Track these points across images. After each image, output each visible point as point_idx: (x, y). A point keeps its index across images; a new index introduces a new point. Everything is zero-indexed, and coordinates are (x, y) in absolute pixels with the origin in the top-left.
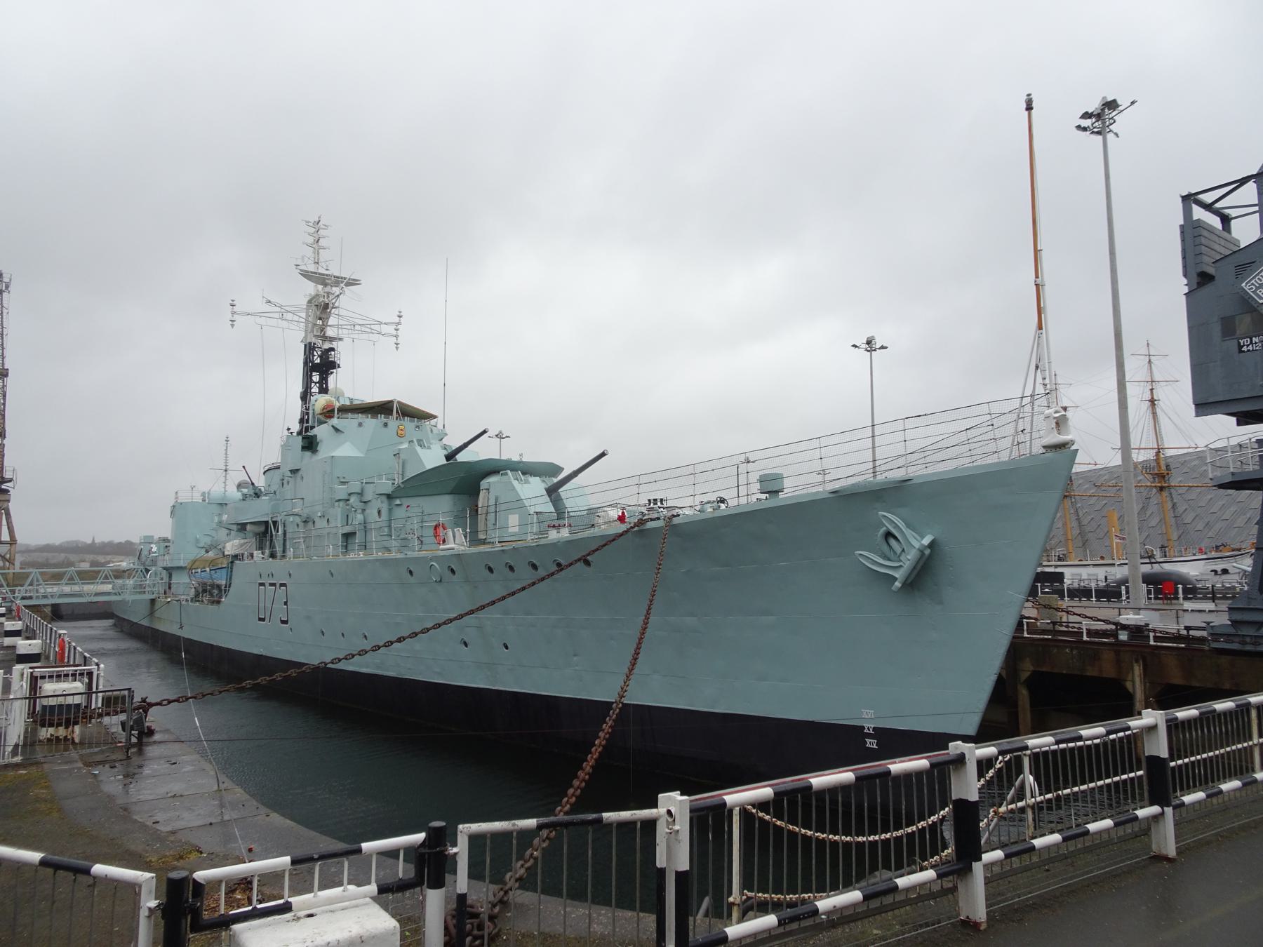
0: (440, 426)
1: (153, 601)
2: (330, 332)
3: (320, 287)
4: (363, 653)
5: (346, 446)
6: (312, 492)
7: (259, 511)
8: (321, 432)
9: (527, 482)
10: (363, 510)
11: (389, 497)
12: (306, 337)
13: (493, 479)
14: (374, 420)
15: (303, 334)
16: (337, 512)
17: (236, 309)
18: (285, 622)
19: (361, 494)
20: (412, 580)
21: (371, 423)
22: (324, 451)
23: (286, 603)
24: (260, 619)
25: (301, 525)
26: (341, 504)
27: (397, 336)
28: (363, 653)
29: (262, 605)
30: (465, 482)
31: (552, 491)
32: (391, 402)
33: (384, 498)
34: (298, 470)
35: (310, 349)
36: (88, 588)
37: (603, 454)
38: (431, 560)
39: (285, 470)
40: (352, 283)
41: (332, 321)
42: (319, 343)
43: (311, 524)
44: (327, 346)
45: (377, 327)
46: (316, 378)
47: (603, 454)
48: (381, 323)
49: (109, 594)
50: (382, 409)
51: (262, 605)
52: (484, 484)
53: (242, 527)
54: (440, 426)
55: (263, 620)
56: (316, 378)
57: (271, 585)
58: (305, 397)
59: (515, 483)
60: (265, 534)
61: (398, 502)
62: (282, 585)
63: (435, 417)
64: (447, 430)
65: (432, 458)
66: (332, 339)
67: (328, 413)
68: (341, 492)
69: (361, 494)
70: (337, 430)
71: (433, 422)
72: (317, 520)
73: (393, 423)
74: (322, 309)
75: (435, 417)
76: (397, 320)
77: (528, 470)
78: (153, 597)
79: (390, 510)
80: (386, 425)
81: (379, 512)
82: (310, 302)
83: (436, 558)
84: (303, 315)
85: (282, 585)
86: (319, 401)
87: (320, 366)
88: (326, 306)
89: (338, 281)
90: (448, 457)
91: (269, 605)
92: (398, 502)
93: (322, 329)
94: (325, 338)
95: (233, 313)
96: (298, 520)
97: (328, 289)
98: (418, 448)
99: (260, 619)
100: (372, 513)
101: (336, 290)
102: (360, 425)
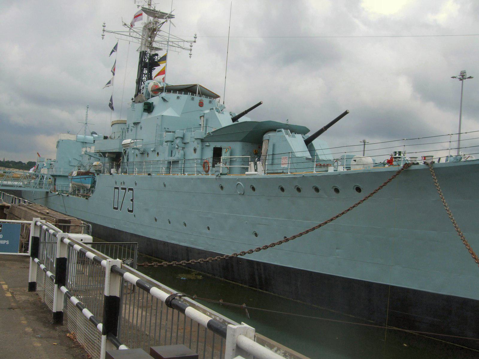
0: (221, 103)
1: (47, 193)
2: (155, 45)
3: (151, 19)
4: (251, 252)
5: (170, 109)
6: (147, 134)
7: (113, 146)
8: (155, 100)
9: (294, 137)
10: (183, 148)
11: (202, 140)
12: (141, 47)
13: (271, 134)
14: (186, 96)
15: (140, 45)
16: (166, 147)
17: (105, 29)
18: (131, 211)
19: (183, 138)
20: (222, 192)
21: (185, 97)
22: (156, 113)
23: (132, 200)
24: (115, 208)
25: (139, 155)
26: (169, 144)
27: (191, 50)
28: (251, 252)
29: (116, 200)
30: (253, 136)
31: (308, 142)
32: (195, 85)
33: (199, 141)
34: (138, 123)
35: (143, 54)
36: (16, 183)
37: (346, 113)
38: (238, 180)
39: (130, 123)
40: (171, 16)
41: (156, 39)
42: (149, 50)
43: (146, 155)
44: (153, 52)
45: (181, 44)
46: (145, 71)
47: (346, 113)
48: (184, 41)
49: (20, 187)
50: (190, 90)
51: (116, 200)
52: (266, 136)
53: (104, 154)
54: (221, 103)
55: (117, 209)
56: (145, 71)
57: (123, 189)
58: (139, 81)
59: (287, 136)
60: (116, 158)
61: (207, 144)
62: (130, 189)
63: (219, 97)
64: (226, 105)
65: (225, 121)
66: (157, 49)
67: (157, 90)
68: (169, 136)
69: (183, 138)
70: (164, 100)
71: (218, 99)
72: (150, 153)
73: (197, 98)
74: (152, 31)
75: (219, 97)
76: (105, 33)
77: (295, 130)
78: (47, 191)
79: (202, 149)
80: (193, 99)
81: (195, 150)
82: (145, 26)
83: (242, 180)
84: (141, 34)
85: (130, 189)
86: (150, 84)
87: (149, 63)
88: (155, 30)
89: (162, 15)
90: (235, 119)
91: (121, 200)
92: (207, 144)
93: (151, 43)
94: (152, 48)
95: (104, 31)
96: (137, 152)
97: (156, 19)
98: (217, 113)
99: (115, 208)
100: (190, 150)
101: (162, 21)
102: (178, 98)
